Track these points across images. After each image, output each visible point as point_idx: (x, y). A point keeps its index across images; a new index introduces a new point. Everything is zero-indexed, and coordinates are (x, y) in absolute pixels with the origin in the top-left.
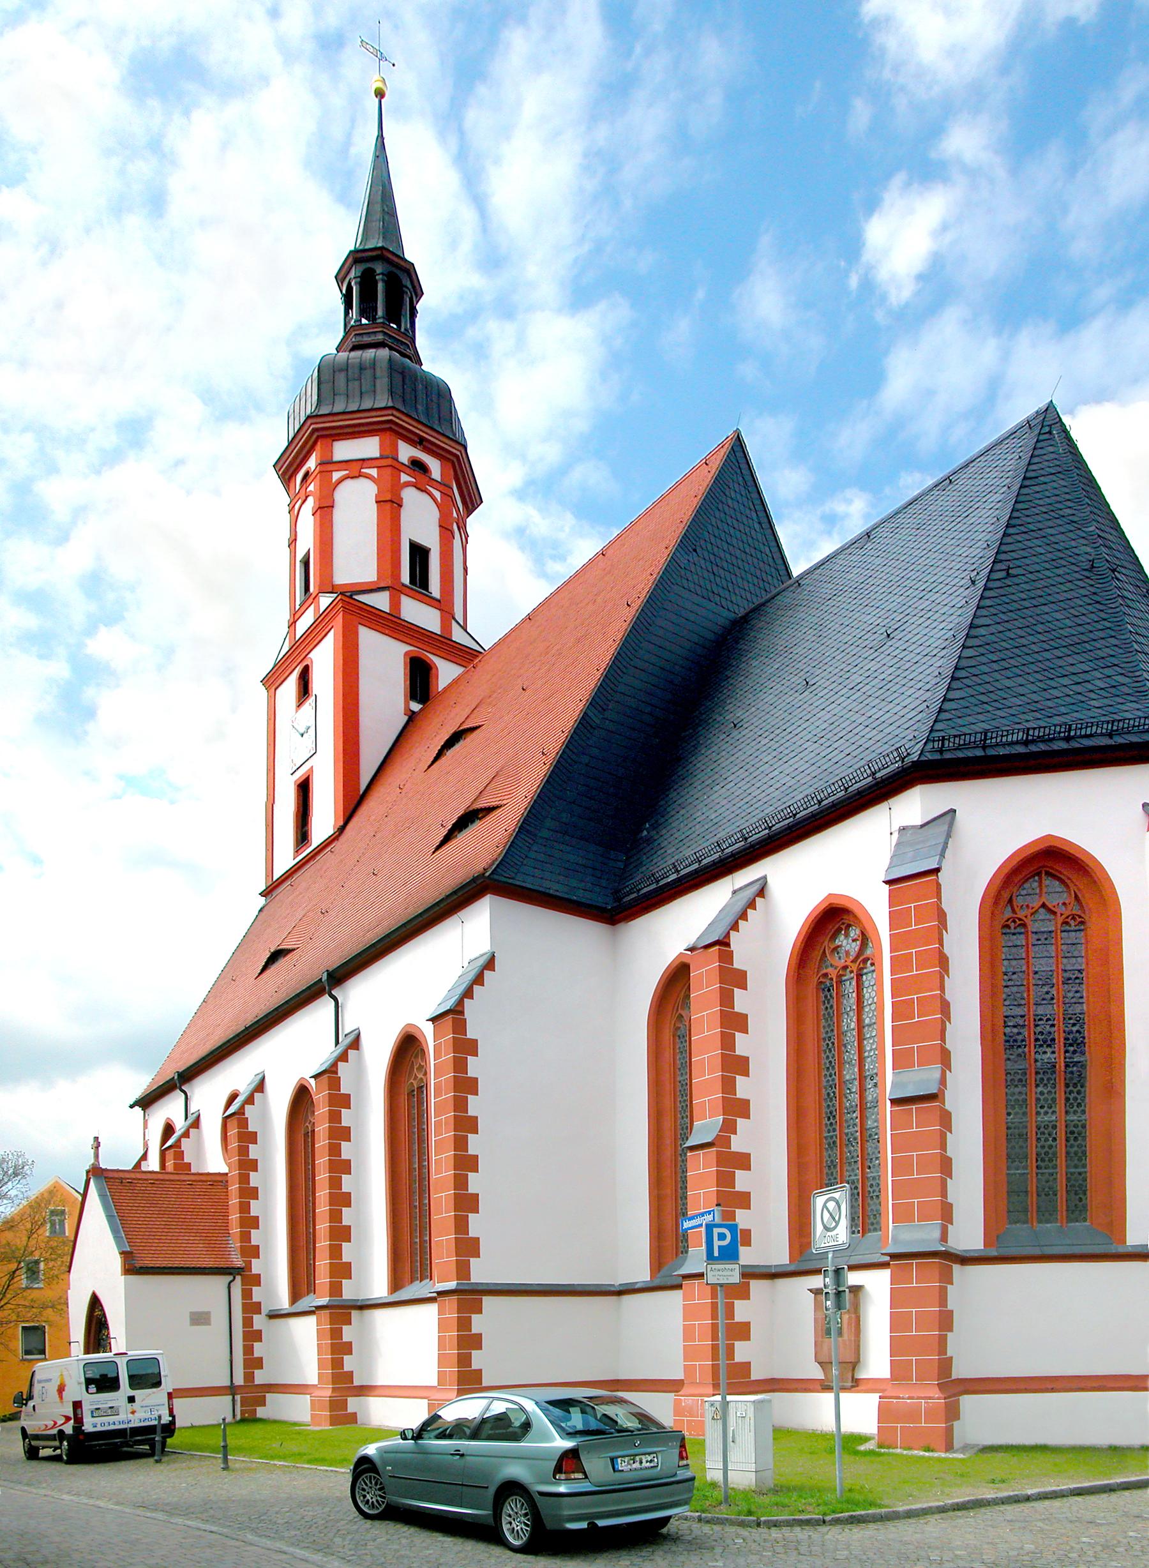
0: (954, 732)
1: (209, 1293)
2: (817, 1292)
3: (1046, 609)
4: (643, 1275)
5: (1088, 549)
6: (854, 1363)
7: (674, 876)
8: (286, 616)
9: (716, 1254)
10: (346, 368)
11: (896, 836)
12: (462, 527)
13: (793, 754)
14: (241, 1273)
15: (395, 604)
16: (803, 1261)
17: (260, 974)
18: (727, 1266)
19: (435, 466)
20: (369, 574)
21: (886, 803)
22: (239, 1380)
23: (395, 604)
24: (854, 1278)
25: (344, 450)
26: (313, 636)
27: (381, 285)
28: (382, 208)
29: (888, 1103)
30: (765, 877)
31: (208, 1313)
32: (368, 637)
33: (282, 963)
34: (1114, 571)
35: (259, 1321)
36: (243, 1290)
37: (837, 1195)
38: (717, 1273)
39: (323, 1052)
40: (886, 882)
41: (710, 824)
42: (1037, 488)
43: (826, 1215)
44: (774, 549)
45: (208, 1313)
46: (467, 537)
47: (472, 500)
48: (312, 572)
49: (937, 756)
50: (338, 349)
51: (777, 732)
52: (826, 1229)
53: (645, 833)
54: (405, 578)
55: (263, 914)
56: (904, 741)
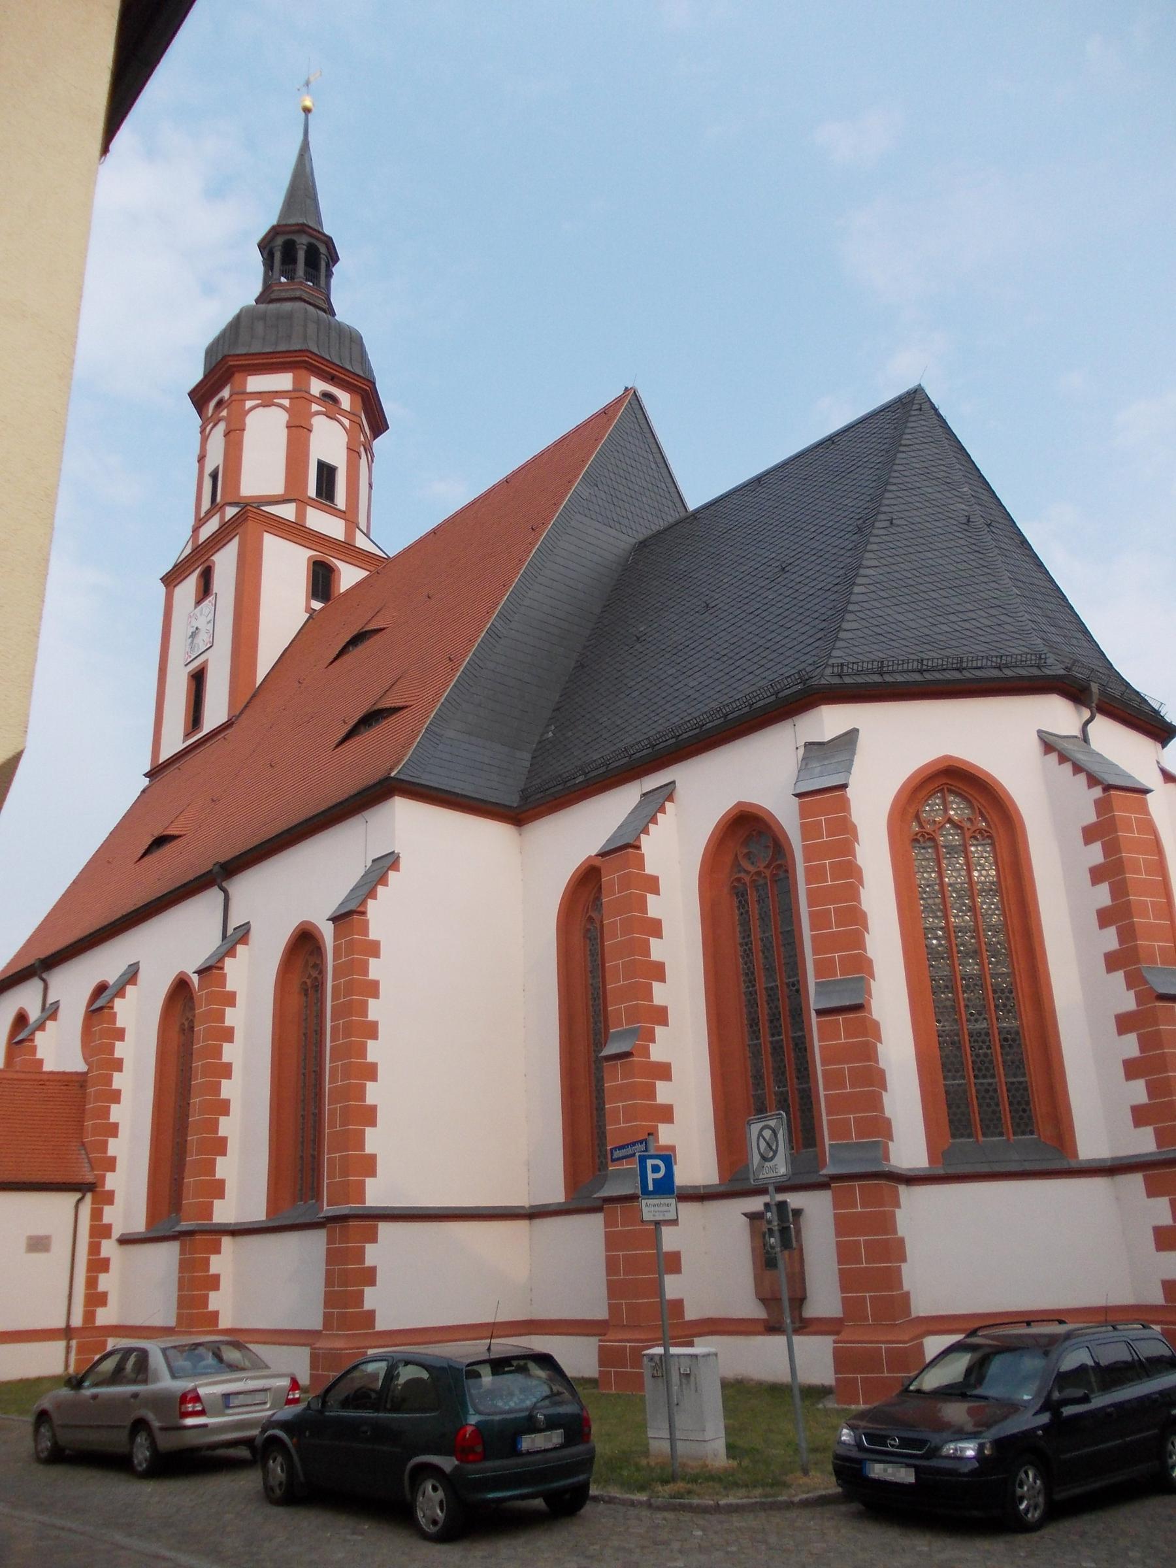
0: (852, 660)
1: (53, 1212)
2: (753, 1217)
3: (929, 555)
4: (556, 1194)
5: (964, 507)
6: (799, 1300)
7: (581, 778)
8: (191, 521)
9: (651, 1188)
10: (263, 317)
11: (801, 751)
12: (369, 449)
13: (697, 669)
14: (89, 1188)
15: (301, 514)
16: (735, 1183)
17: (142, 857)
18: (663, 1201)
19: (345, 399)
20: (277, 487)
21: (790, 720)
22: (77, 1321)
23: (301, 514)
24: (794, 1200)
25: (257, 383)
26: (218, 541)
27: (298, 253)
28: (302, 190)
29: (813, 1014)
30: (673, 782)
31: (48, 1238)
32: (273, 545)
33: (167, 850)
34: (989, 525)
35: (108, 1248)
36: (93, 1210)
37: (772, 1123)
38: (652, 1209)
39: (207, 942)
40: (796, 795)
41: (617, 729)
42: (912, 454)
43: (763, 1145)
44: (670, 485)
45: (48, 1238)
46: (373, 456)
47: (379, 425)
48: (221, 483)
49: (836, 680)
50: (257, 301)
51: (680, 647)
52: (764, 1158)
53: (550, 734)
54: (312, 491)
55: (145, 795)
56: (804, 665)
